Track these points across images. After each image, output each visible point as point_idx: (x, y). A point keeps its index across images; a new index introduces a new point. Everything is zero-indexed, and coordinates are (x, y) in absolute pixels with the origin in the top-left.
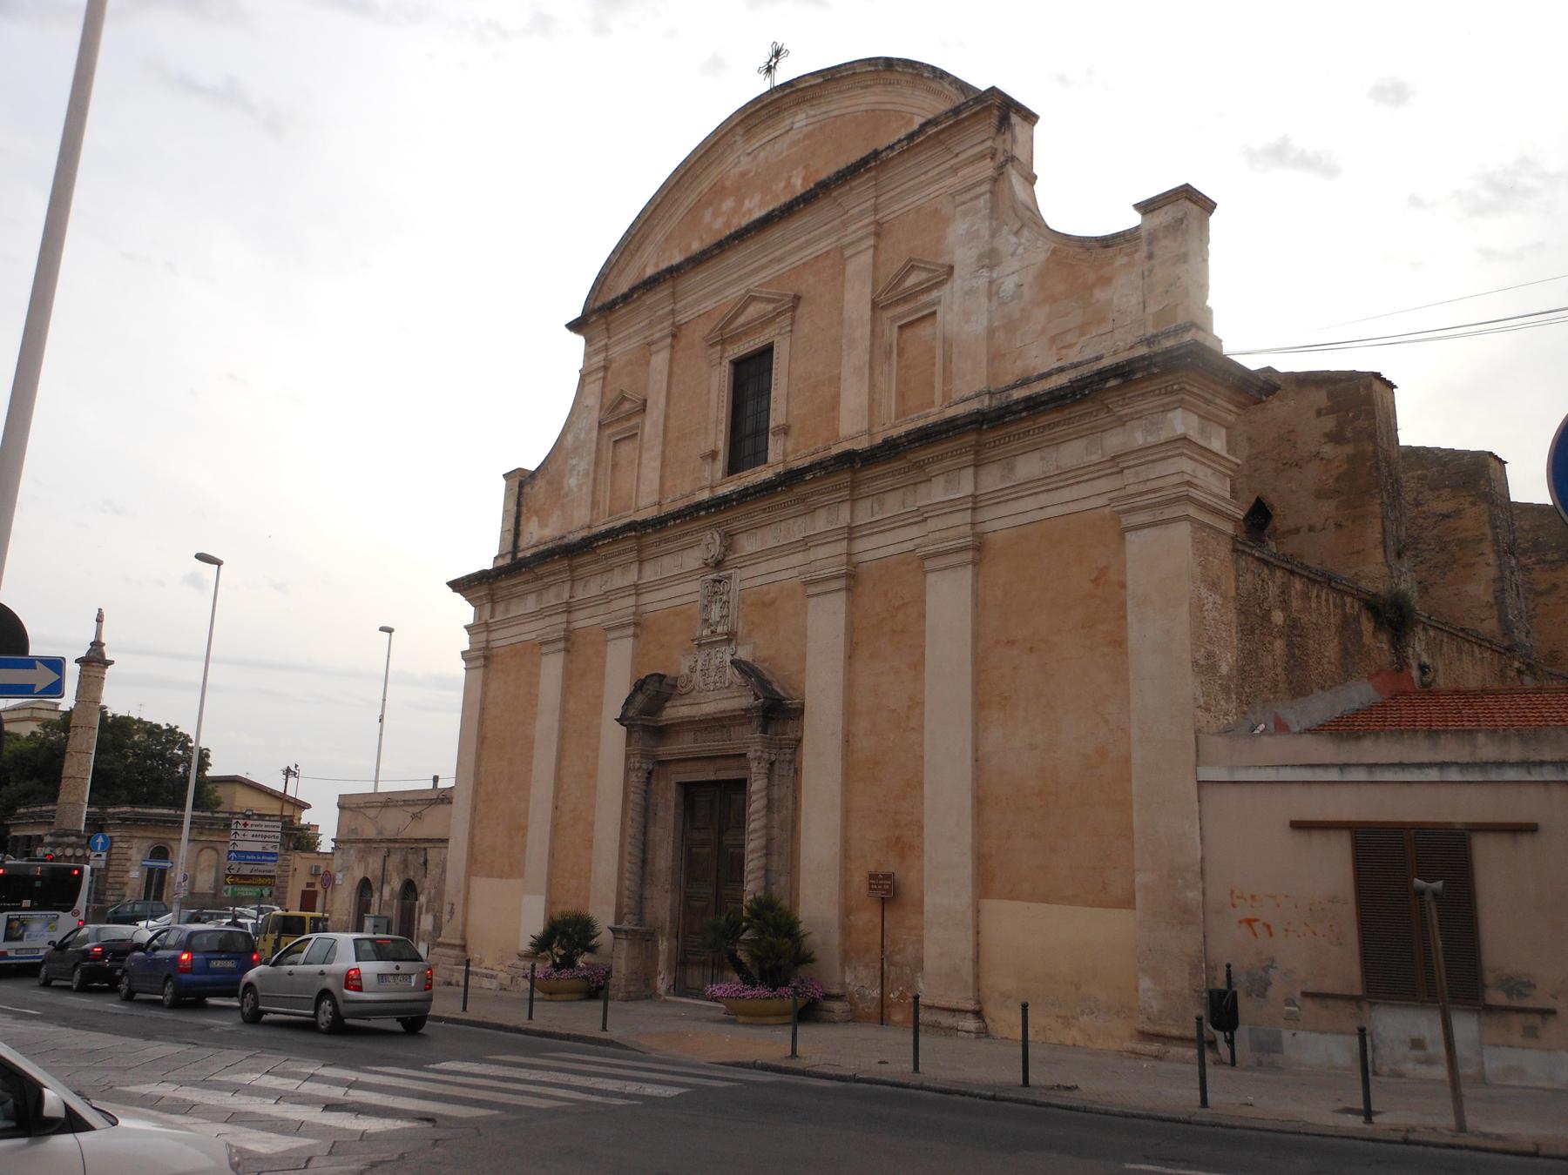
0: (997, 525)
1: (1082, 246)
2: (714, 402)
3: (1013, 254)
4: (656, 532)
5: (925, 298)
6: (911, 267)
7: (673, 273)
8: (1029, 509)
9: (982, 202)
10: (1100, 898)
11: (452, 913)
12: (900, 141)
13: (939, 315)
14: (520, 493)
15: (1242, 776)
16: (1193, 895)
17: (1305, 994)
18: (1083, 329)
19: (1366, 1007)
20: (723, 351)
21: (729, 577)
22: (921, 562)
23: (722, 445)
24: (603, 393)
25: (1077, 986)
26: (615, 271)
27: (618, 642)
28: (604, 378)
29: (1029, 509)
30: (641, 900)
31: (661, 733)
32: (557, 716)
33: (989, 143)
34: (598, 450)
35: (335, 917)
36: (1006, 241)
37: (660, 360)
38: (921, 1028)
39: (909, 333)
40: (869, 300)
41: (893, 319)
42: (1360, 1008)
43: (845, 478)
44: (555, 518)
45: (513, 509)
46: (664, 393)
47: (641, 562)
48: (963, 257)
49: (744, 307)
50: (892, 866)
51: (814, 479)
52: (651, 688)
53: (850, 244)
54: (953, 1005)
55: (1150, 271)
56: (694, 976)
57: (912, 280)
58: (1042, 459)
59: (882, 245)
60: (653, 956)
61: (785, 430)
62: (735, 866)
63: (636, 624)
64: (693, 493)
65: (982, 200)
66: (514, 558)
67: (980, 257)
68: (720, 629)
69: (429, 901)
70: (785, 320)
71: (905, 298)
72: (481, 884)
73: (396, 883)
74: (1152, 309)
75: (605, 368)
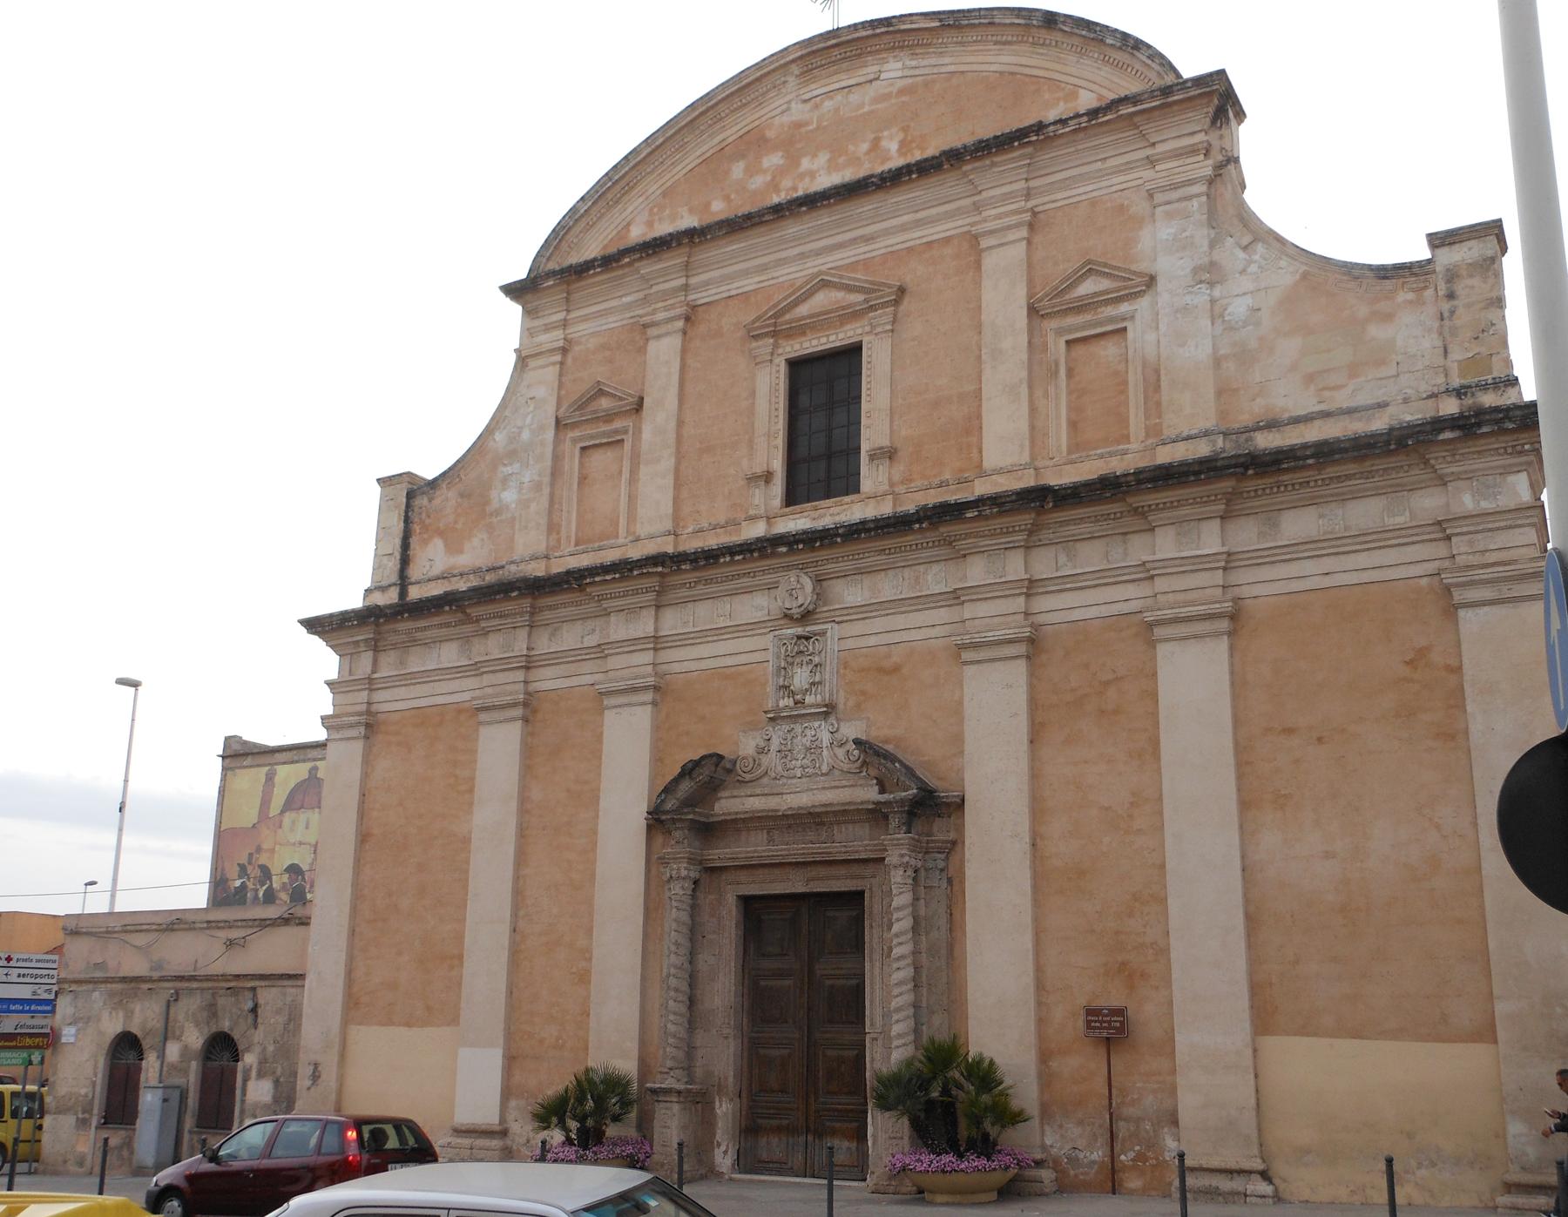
1: (1349, 273)
3: (1243, 272)
4: (695, 569)
5: (1110, 311)
6: (1090, 269)
7: (692, 237)
8: (1309, 573)
10: (1439, 1031)
11: (315, 1077)
12: (1077, 116)
13: (1130, 334)
14: (408, 506)
18: (1353, 370)
20: (776, 346)
21: (823, 633)
23: (778, 465)
24: (561, 386)
26: (582, 224)
27: (626, 711)
29: (1309, 573)
30: (690, 1050)
31: (708, 831)
32: (514, 805)
33: (1200, 137)
34: (557, 458)
35: (62, 1089)
36: (1231, 255)
37: (664, 350)
38: (1189, 1195)
39: (1080, 350)
40: (1023, 302)
43: (1026, 519)
44: (476, 541)
45: (399, 527)
47: (658, 607)
48: (1172, 268)
52: (704, 774)
53: (991, 232)
54: (1232, 1165)
55: (1452, 312)
56: (772, 1146)
57: (1087, 287)
59: (1037, 239)
60: (707, 1122)
61: (888, 454)
62: (850, 1004)
63: (656, 688)
64: (735, 523)
65: (1195, 203)
66: (403, 593)
67: (1196, 270)
68: (809, 699)
69: (263, 1061)
70: (883, 317)
71: (1081, 308)
73: (195, 1038)
74: (1457, 354)
75: (564, 351)
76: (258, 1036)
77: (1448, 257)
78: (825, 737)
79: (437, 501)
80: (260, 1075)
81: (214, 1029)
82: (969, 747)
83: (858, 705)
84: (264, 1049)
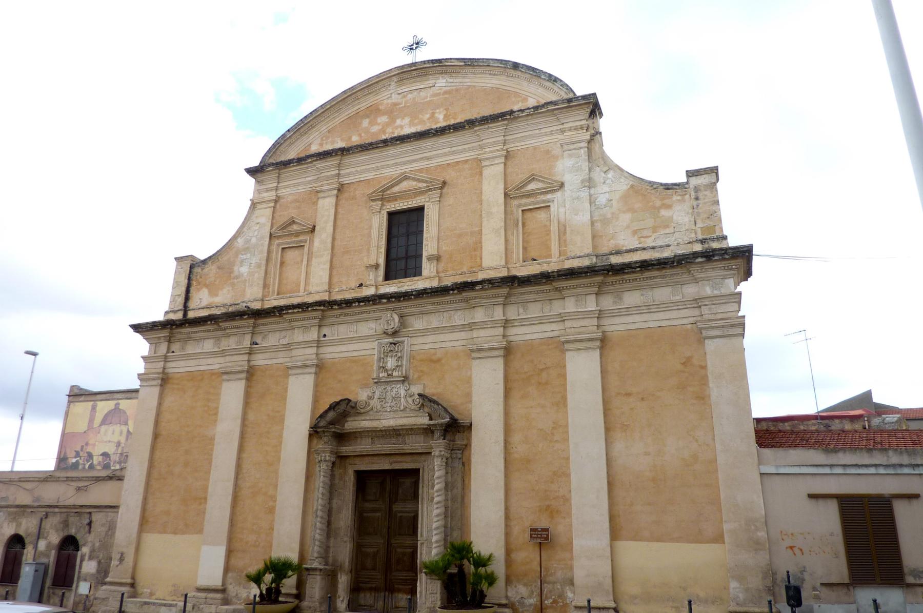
0: (614, 328)
2: (375, 233)
4: (340, 309)
5: (542, 197)
6: (532, 178)
8: (637, 321)
9: (582, 151)
10: (698, 538)
11: (121, 560)
12: (529, 108)
13: (552, 209)
14: (190, 272)
15: (782, 471)
16: (762, 534)
17: (822, 584)
18: (655, 229)
19: (851, 588)
20: (383, 205)
21: (403, 342)
22: (561, 345)
23: (382, 261)
24: (273, 218)
25: (685, 589)
26: (288, 142)
28: (274, 207)
36: (598, 175)
39: (528, 215)
41: (518, 206)
42: (849, 589)
46: (331, 223)
49: (530, 182)
50: (543, 523)
51: (483, 289)
53: (487, 159)
57: (532, 186)
58: (642, 295)
61: (437, 258)
66: (185, 314)
67: (582, 181)
68: (395, 374)
69: (92, 551)
70: (436, 194)
72: (152, 540)
73: (55, 538)
75: (276, 201)
76: (90, 538)
77: (694, 181)
78: (402, 392)
79: (206, 270)
80: (91, 558)
81: (66, 534)
82: (475, 398)
83: (419, 377)
84: (94, 545)
